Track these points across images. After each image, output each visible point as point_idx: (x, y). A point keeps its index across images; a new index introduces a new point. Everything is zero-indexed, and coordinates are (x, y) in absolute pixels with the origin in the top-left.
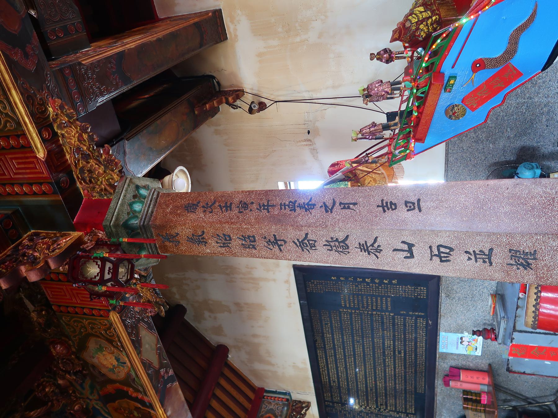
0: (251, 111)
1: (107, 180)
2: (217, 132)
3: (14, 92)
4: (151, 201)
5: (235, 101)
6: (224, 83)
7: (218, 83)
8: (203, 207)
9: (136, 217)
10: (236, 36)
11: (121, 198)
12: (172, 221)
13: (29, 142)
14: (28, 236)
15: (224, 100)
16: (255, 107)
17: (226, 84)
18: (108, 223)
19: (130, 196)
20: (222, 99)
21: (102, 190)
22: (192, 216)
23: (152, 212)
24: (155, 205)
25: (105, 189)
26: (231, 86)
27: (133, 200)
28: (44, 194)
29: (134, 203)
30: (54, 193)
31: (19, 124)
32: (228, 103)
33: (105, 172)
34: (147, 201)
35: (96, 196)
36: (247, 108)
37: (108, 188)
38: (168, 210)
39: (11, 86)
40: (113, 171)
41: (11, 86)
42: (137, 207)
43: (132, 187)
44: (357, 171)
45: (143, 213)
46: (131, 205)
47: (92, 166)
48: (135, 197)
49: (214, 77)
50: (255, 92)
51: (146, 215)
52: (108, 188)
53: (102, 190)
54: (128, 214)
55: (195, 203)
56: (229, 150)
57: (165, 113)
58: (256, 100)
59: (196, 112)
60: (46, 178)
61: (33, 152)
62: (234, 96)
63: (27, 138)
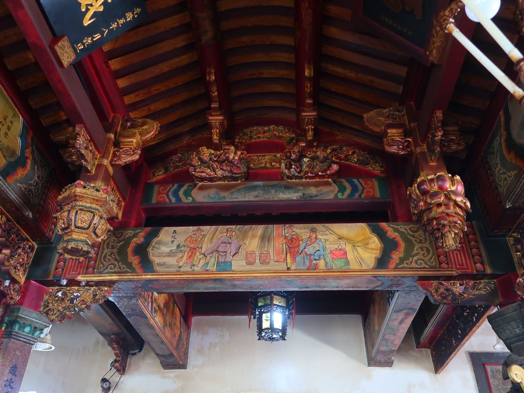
0: (104, 380)
1: (54, 310)
2: (97, 342)
3: (118, 277)
4: (29, 340)
5: (115, 368)
6: (134, 358)
7: (135, 354)
8: (11, 379)
9: (20, 329)
10: (165, 377)
11: (37, 321)
12: (8, 355)
13: (88, 274)
14: (33, 245)
15: (118, 359)
16: (106, 384)
17: (132, 360)
18: (20, 312)
19: (37, 325)
20: (120, 357)
21: (48, 303)
22: (7, 371)
23: (20, 340)
24: (25, 342)
25: (48, 306)
26: (130, 364)
27: (33, 326)
28: (56, 269)
29: (31, 327)
30: (54, 276)
31: (100, 273)
32: (116, 361)
33: (59, 311)
34: (29, 337)
35: (46, 297)
36: (107, 377)
37: (47, 309)
38: (17, 352)
39: (121, 277)
40: (57, 317)
41: (121, 277)
42: (27, 329)
43: (42, 327)
44: (162, 306)
45: (21, 334)
46: (30, 325)
47: (65, 303)
48: (35, 328)
49: (140, 350)
50: (120, 384)
51: (19, 337)
52: (47, 309)
53: (48, 303)
54: (24, 324)
55: (16, 373)
56: (79, 350)
57: (113, 319)
58: (113, 385)
59: (112, 336)
60: (65, 275)
61: (82, 274)
62: (119, 368)
63: (91, 273)
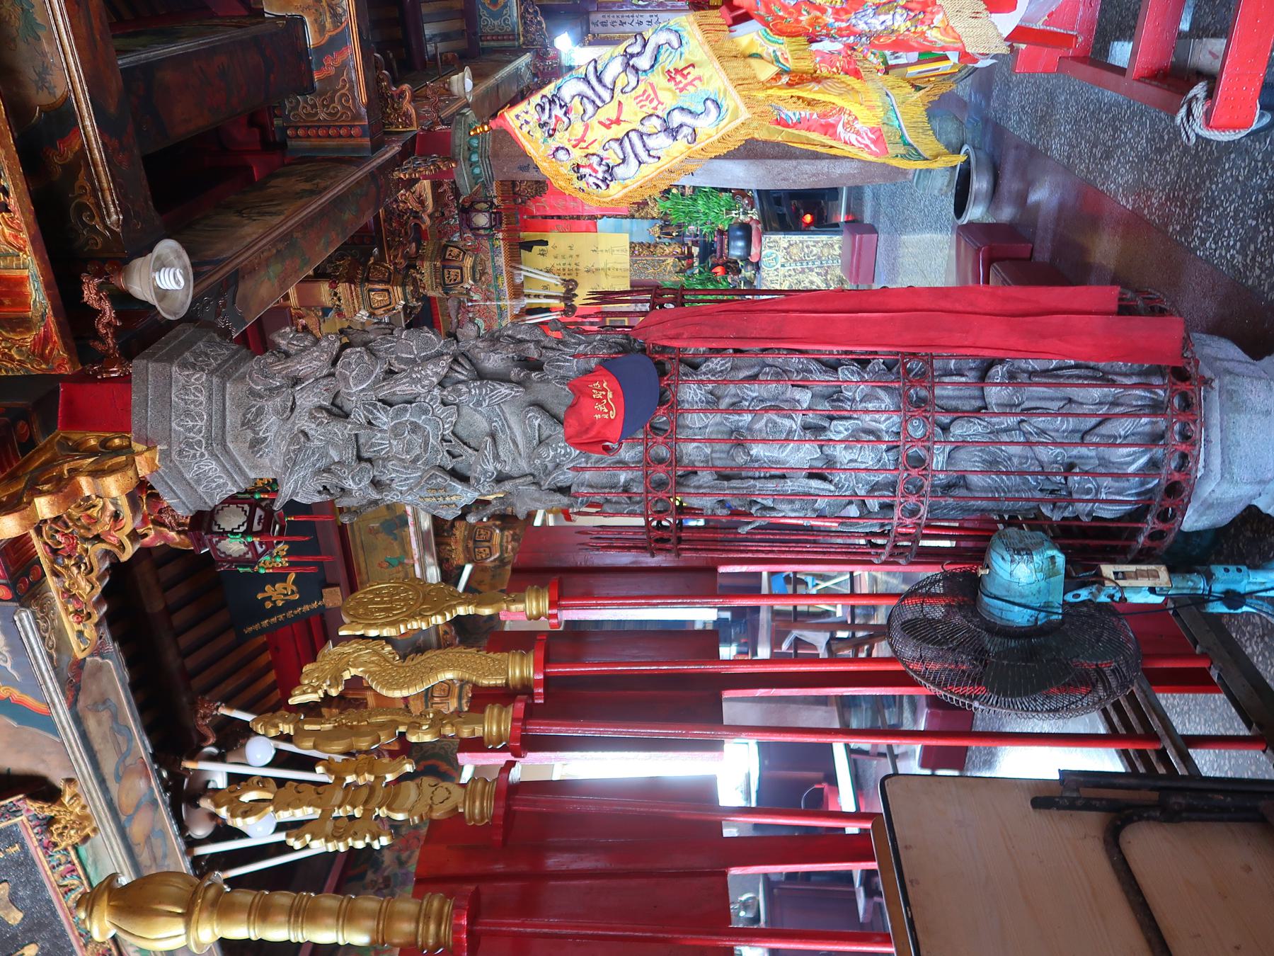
42: (477, 171)
